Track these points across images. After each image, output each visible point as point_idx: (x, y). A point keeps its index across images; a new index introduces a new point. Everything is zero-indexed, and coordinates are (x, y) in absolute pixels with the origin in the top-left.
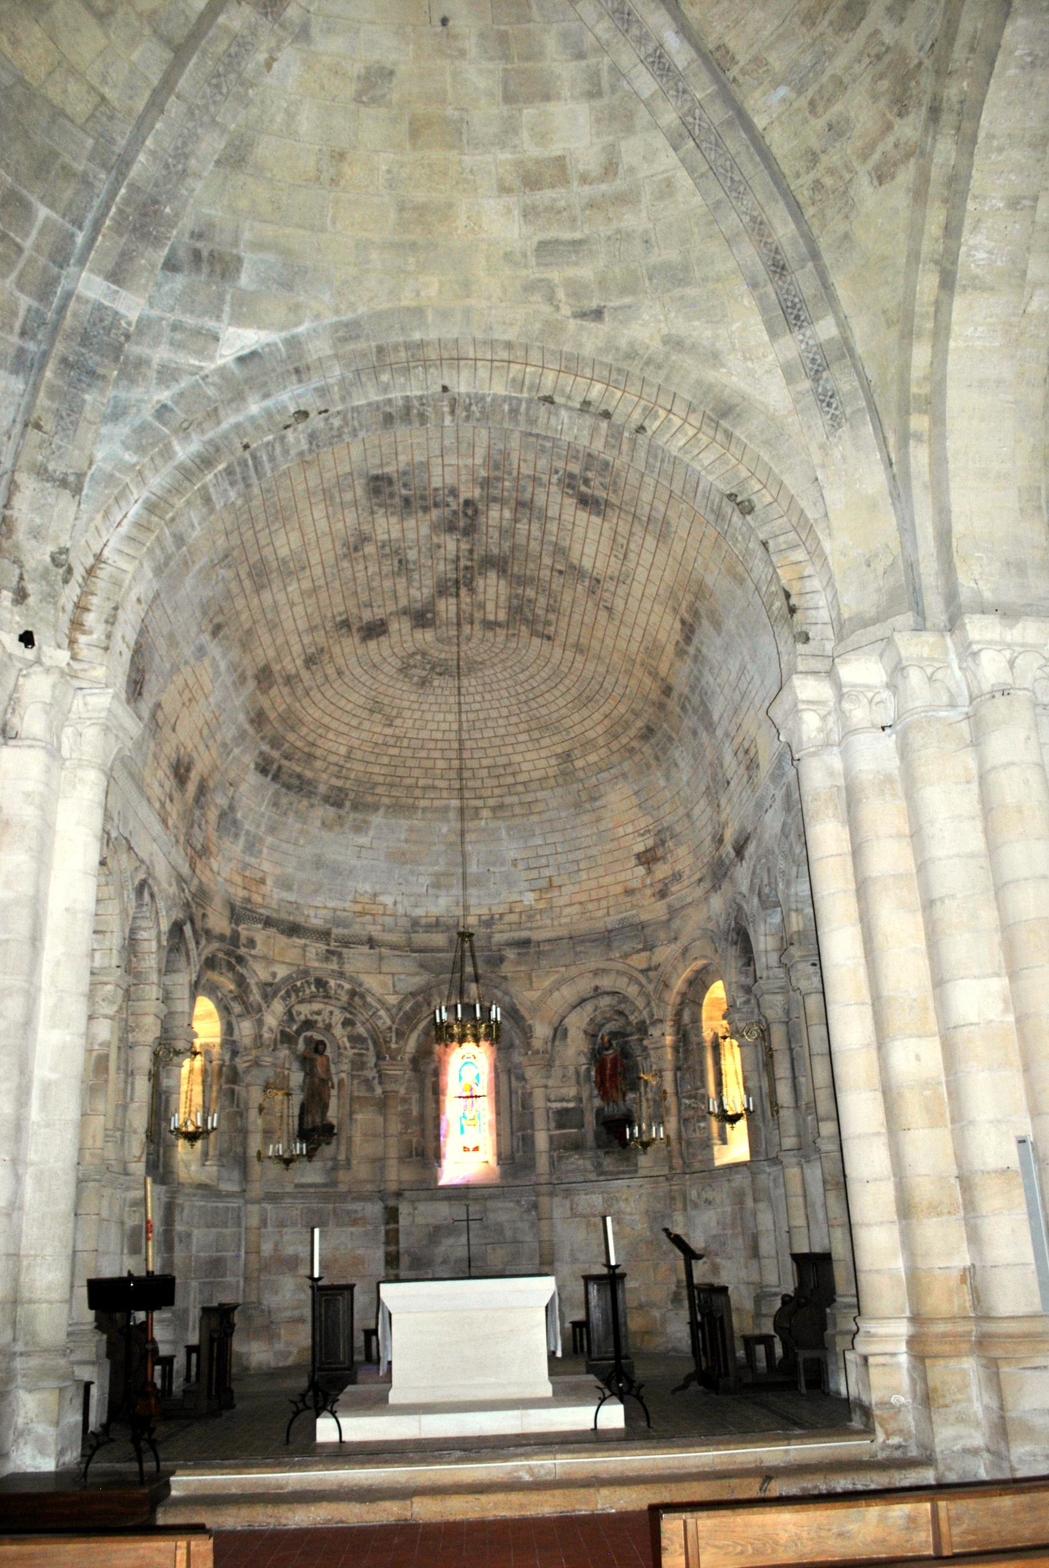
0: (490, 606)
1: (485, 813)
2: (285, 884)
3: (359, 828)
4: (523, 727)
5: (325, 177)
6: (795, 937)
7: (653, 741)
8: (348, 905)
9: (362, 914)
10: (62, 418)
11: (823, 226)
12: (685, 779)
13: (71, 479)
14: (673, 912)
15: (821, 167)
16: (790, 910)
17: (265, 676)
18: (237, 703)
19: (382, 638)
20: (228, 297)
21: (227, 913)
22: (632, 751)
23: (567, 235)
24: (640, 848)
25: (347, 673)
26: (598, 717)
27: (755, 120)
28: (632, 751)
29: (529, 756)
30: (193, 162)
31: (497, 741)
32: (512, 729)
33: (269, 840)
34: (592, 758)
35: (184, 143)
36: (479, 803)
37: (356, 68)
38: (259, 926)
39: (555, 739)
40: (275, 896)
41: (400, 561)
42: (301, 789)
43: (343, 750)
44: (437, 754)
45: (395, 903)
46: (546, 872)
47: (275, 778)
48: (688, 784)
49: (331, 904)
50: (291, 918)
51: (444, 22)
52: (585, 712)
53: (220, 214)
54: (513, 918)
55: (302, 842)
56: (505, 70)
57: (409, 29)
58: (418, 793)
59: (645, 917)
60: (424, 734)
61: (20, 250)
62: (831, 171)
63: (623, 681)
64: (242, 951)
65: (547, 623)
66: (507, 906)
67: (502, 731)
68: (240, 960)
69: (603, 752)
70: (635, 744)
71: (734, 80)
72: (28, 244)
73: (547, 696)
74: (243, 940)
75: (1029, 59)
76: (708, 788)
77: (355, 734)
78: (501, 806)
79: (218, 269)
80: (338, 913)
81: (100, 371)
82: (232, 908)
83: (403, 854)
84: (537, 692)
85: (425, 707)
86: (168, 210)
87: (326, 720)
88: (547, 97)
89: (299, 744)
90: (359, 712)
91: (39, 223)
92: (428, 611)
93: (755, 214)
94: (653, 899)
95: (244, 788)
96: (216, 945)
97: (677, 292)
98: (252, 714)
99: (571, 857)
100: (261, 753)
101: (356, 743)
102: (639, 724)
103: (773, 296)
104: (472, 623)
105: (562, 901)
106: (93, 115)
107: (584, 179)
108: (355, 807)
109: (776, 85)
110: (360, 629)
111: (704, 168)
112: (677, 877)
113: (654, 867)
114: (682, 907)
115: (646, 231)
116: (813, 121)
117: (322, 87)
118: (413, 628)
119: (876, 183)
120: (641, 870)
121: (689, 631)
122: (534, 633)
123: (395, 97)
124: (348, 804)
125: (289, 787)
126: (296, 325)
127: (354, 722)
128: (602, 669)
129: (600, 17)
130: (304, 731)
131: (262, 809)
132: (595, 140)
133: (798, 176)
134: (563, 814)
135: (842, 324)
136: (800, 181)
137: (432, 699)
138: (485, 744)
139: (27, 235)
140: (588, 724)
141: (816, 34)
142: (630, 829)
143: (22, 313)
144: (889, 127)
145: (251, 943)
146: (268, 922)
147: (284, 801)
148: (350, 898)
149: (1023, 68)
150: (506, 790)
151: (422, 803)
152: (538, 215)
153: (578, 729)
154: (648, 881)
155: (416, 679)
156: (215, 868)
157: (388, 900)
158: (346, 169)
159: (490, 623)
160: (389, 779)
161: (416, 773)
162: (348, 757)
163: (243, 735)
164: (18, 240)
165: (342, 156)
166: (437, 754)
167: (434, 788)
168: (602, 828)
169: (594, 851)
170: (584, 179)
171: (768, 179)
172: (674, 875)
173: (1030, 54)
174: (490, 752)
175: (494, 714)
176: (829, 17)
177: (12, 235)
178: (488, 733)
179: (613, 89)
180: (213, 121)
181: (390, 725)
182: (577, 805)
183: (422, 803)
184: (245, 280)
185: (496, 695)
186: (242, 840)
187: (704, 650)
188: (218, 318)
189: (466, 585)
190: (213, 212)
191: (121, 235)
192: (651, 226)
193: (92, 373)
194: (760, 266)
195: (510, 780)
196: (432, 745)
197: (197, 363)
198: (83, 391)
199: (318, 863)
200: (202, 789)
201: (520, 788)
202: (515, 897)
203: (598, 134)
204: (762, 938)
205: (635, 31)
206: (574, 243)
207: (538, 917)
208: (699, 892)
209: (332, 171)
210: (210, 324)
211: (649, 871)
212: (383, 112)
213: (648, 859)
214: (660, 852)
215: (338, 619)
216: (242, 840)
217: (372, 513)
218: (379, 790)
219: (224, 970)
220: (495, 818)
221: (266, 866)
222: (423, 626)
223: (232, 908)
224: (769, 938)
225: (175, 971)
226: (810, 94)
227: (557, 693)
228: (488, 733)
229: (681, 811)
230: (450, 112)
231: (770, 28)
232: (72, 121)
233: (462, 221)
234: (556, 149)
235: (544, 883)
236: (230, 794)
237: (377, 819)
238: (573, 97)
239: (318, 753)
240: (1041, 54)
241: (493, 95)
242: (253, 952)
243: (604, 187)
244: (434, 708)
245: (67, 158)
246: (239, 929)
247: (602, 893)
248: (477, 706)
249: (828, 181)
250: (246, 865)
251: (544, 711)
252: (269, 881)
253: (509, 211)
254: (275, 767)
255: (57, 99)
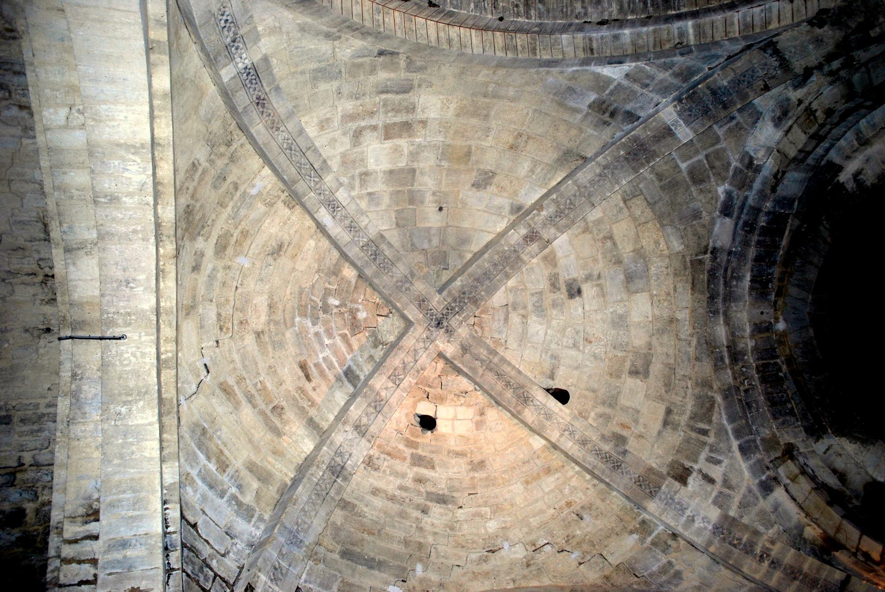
5: (524, 138)
10: (749, 82)
11: (224, 120)
13: (770, 51)
15: (229, 155)
20: (607, 92)
23: (389, 96)
27: (270, 171)
30: (598, 171)
35: (599, 181)
37: (492, 189)
51: (441, 209)
53: (589, 130)
56: (412, 185)
57: (460, 206)
61: (707, 157)
62: (222, 155)
71: (283, 192)
72: (701, 157)
75: (132, 285)
79: (604, 106)
81: (708, 92)
86: (622, 153)
88: (391, 172)
91: (689, 162)
93: (276, 133)
97: (323, 65)
103: (264, 85)
106: (634, 197)
107: (374, 128)
109: (260, 193)
111: (308, 154)
115: (340, 99)
116: (235, 179)
117: (511, 182)
119: (196, 162)
123: (474, 174)
126: (577, 71)
129: (366, 228)
132: (365, 149)
133: (242, 145)
135: (217, 80)
136: (239, 143)
139: (699, 161)
141: (240, 227)
143: (726, 127)
144: (193, 197)
149: (134, 280)
152: (407, 108)
158: (511, 140)
164: (705, 162)
165: (511, 148)
170: (374, 128)
171: (269, 155)
173: (132, 288)
176: (235, 238)
177: (707, 166)
179: (353, 177)
180: (579, 187)
184: (593, 97)
188: (619, 84)
190: (592, 132)
191: (654, 151)
192: (336, 103)
193: (714, 93)
194: (274, 101)
197: (646, 67)
198: (725, 87)
203: (363, 152)
205: (347, 222)
206: (387, 92)
209: (519, 140)
210: (625, 83)
212: (482, 167)
226: (238, 194)
230: (445, 164)
231: (266, 224)
232: (646, 199)
233: (453, 106)
234: (389, 144)
238: (377, 173)
240: (124, 288)
241: (421, 173)
243: (363, 124)
245: (657, 183)
249: (223, 149)
253: (423, 111)
255: (648, 210)
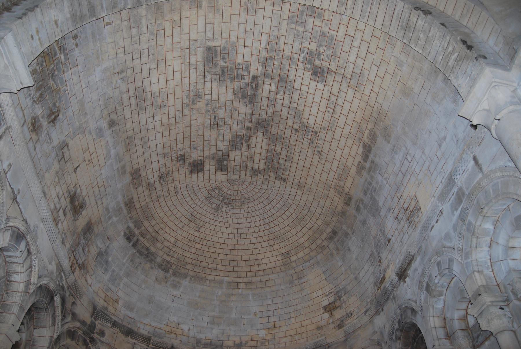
0: (257, 159)
1: (242, 286)
2: (129, 307)
3: (175, 286)
4: (266, 238)
6: (482, 289)
7: (336, 239)
8: (162, 326)
9: (170, 333)
12: (354, 257)
14: (348, 336)
16: (474, 271)
17: (146, 271)
18: (119, 186)
19: (200, 174)
21: (90, 309)
22: (323, 248)
24: (326, 303)
25: (180, 193)
26: (305, 230)
28: (323, 248)
29: (267, 255)
31: (251, 246)
32: (260, 240)
33: (125, 280)
34: (301, 255)
36: (239, 280)
38: (109, 325)
39: (282, 244)
40: (122, 312)
41: (215, 117)
42: (147, 257)
43: (172, 240)
44: (220, 251)
45: (189, 330)
46: (272, 319)
47: (134, 245)
48: (357, 259)
49: (154, 324)
50: (130, 326)
52: (299, 228)
54: (253, 343)
55: (143, 286)
58: (208, 271)
59: (329, 341)
60: (215, 239)
63: (322, 203)
64: (96, 336)
65: (285, 170)
66: (250, 337)
67: (254, 241)
68: (92, 340)
69: (307, 251)
70: (325, 243)
73: (279, 219)
74: (97, 330)
76: (372, 255)
77: (179, 232)
78: (251, 283)
80: (157, 330)
82: (95, 308)
83: (197, 304)
84: (275, 217)
85: (217, 223)
87: (166, 220)
89: (150, 230)
90: (183, 219)
92: (225, 160)
94: (334, 330)
95: (115, 244)
96: (78, 324)
98: (126, 199)
99: (286, 310)
100: (128, 227)
101: (180, 238)
102: (329, 230)
104: (246, 171)
105: (281, 335)
108: (174, 274)
110: (190, 164)
112: (349, 315)
113: (334, 313)
114: (354, 331)
118: (216, 170)
120: (326, 315)
121: (367, 150)
122: (277, 177)
124: (171, 271)
125: (141, 254)
127: (180, 225)
128: (311, 198)
130: (153, 223)
131: (124, 261)
134: (283, 287)
137: (221, 219)
138: (245, 247)
140: (300, 234)
142: (320, 293)
145: (102, 333)
146: (115, 324)
147: (137, 260)
148: (165, 323)
150: (253, 273)
151: (210, 277)
153: (295, 238)
154: (331, 321)
155: (214, 206)
156: (89, 281)
157: (185, 327)
159: (256, 170)
160: (194, 262)
161: (208, 260)
162: (174, 245)
163: (119, 210)
166: (220, 251)
167: (216, 269)
168: (304, 294)
169: (299, 307)
172: (347, 314)
174: (248, 252)
175: (251, 230)
178: (247, 241)
181: (198, 231)
182: (291, 282)
183: (210, 277)
185: (253, 219)
186: (110, 273)
187: (377, 160)
189: (246, 142)
195: (256, 268)
196: (218, 245)
199: (150, 300)
200: (88, 229)
201: (261, 273)
202: (255, 333)
204: (431, 319)
207: (267, 343)
208: (366, 319)
211: (331, 315)
213: (330, 309)
214: (338, 304)
215: (179, 153)
216: (110, 273)
217: (204, 77)
218: (189, 267)
219: (80, 343)
220: (247, 289)
221: (120, 294)
222: (221, 170)
223: (95, 308)
224: (436, 319)
225: (42, 327)
227: (285, 217)
228: (247, 241)
229: (352, 276)
235: (271, 325)
236: (107, 244)
237: (185, 282)
239: (159, 238)
242: (102, 339)
244: (222, 224)
246: (97, 322)
247: (304, 329)
248: (242, 226)
250: (109, 289)
251: (277, 229)
252: (121, 303)
254: (135, 238)
